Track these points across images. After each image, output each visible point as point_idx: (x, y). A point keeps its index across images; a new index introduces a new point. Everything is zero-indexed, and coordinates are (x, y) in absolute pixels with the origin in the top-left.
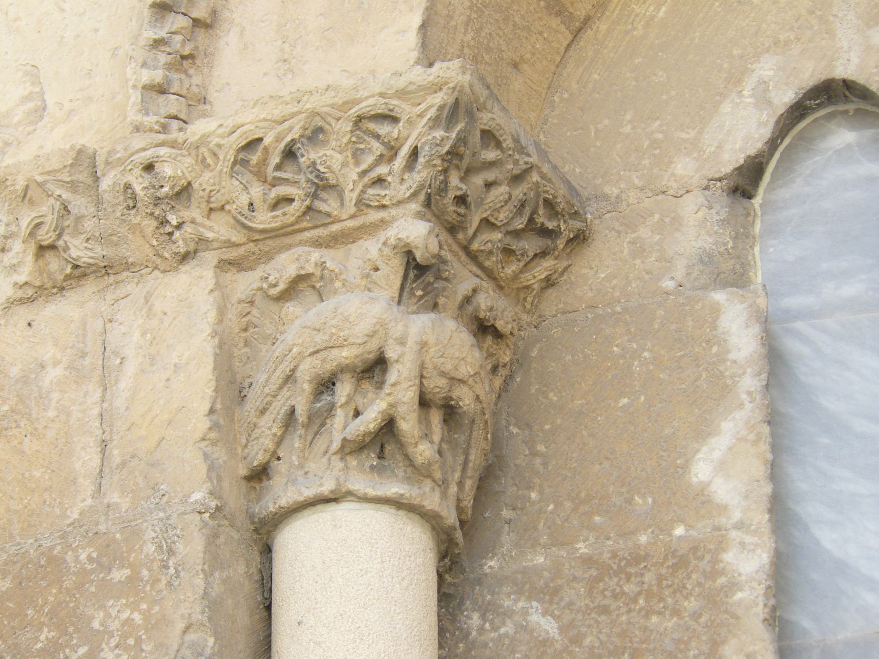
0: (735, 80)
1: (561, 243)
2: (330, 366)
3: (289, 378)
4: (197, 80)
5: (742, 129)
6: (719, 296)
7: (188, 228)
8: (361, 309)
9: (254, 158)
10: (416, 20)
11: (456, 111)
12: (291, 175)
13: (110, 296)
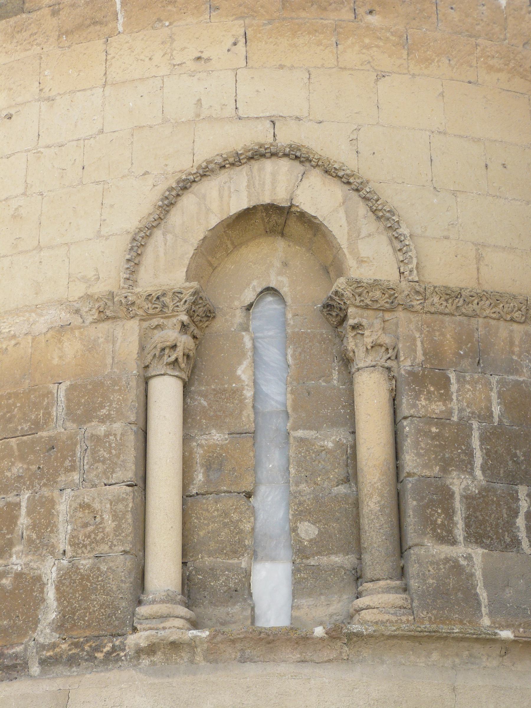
0: (248, 285)
1: (210, 319)
2: (164, 346)
3: (155, 347)
4: (135, 277)
5: (249, 296)
6: (244, 333)
7: (134, 311)
8: (171, 334)
9: (150, 298)
10: (186, 270)
11: (195, 293)
12: (158, 302)
13: (115, 324)
